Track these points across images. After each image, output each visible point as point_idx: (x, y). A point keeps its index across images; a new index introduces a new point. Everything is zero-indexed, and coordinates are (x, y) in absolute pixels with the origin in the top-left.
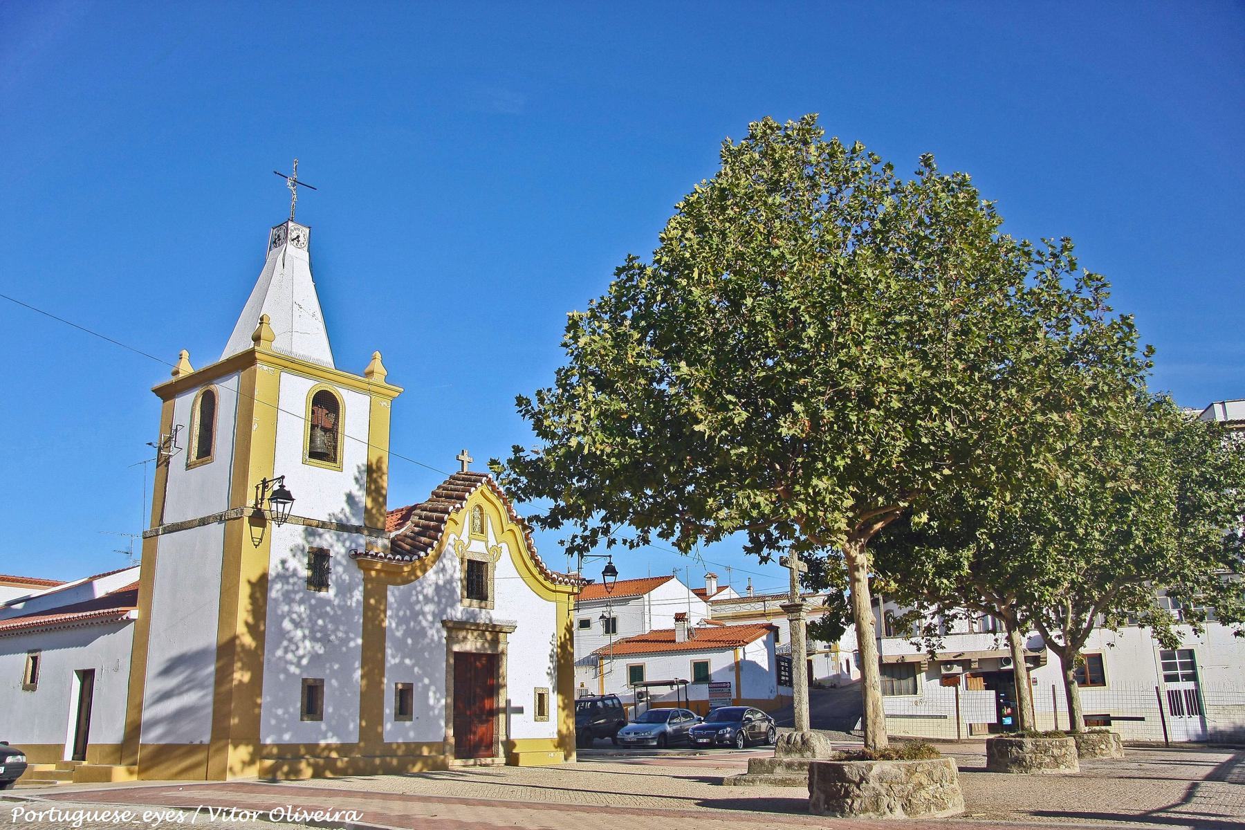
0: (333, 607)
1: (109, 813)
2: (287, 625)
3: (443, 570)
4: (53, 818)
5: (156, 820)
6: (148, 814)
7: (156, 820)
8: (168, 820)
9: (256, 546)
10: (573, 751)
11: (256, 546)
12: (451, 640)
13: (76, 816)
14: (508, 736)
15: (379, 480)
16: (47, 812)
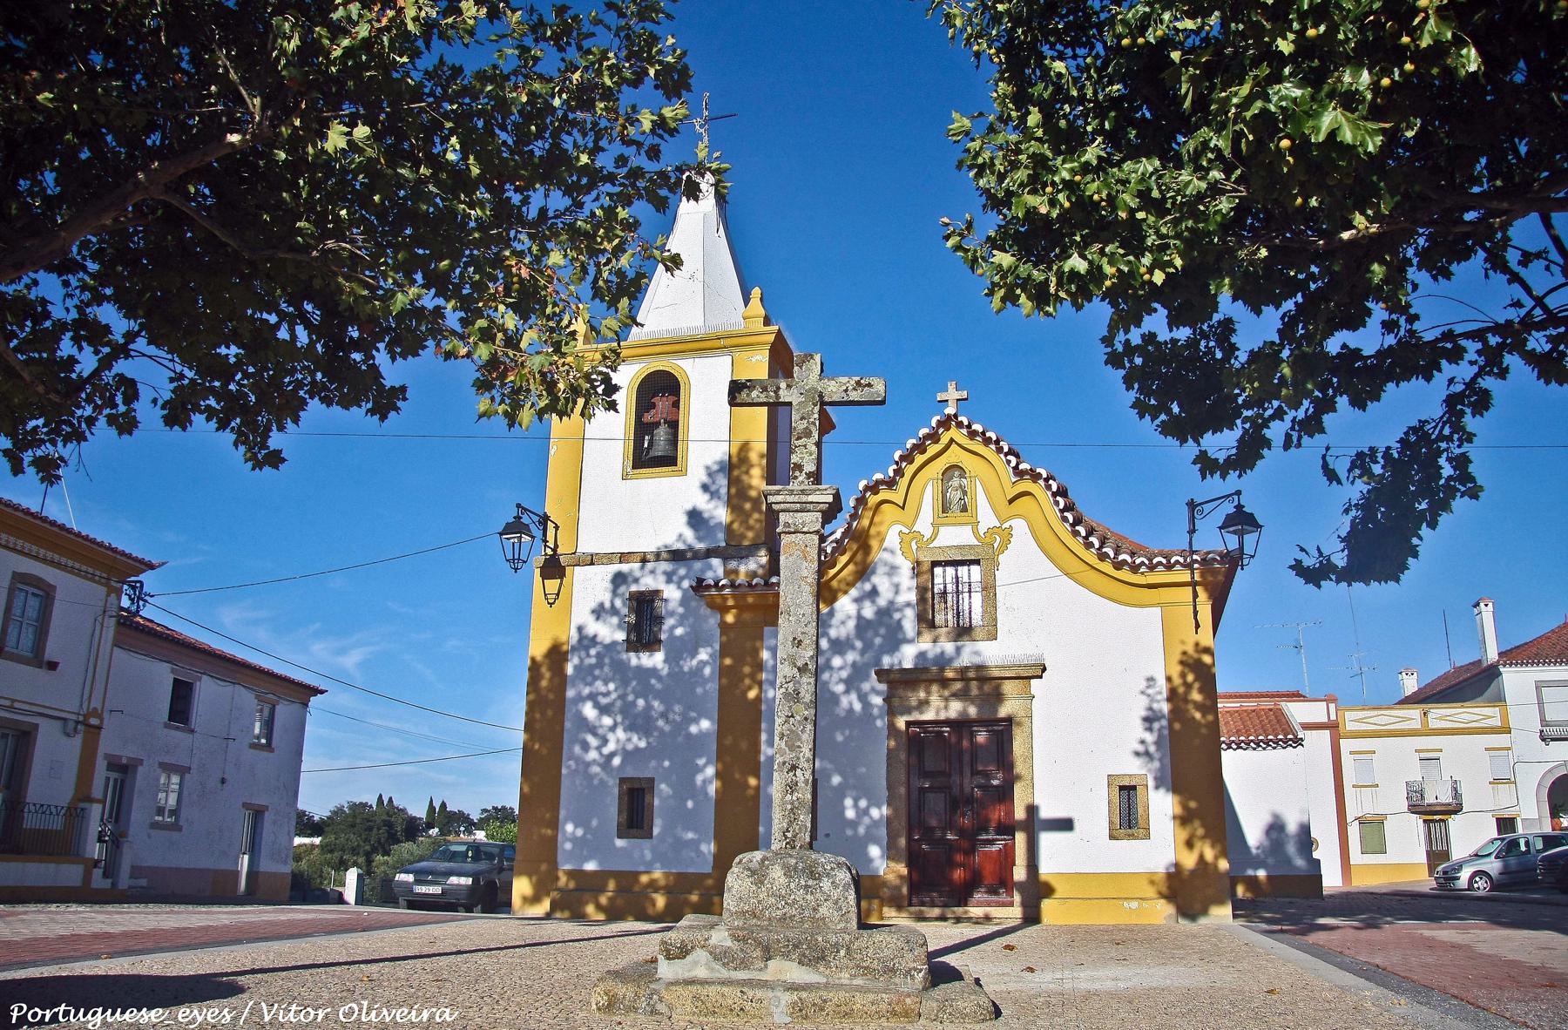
0: (660, 678)
1: (217, 1012)
2: (589, 711)
3: (874, 593)
4: (64, 1018)
5: (194, 1019)
6: (403, 1012)
7: (194, 1019)
8: (399, 1020)
9: (551, 604)
10: (600, 863)
11: (551, 604)
12: (893, 707)
13: (93, 1016)
14: (1032, 866)
15: (745, 478)
16: (56, 1010)
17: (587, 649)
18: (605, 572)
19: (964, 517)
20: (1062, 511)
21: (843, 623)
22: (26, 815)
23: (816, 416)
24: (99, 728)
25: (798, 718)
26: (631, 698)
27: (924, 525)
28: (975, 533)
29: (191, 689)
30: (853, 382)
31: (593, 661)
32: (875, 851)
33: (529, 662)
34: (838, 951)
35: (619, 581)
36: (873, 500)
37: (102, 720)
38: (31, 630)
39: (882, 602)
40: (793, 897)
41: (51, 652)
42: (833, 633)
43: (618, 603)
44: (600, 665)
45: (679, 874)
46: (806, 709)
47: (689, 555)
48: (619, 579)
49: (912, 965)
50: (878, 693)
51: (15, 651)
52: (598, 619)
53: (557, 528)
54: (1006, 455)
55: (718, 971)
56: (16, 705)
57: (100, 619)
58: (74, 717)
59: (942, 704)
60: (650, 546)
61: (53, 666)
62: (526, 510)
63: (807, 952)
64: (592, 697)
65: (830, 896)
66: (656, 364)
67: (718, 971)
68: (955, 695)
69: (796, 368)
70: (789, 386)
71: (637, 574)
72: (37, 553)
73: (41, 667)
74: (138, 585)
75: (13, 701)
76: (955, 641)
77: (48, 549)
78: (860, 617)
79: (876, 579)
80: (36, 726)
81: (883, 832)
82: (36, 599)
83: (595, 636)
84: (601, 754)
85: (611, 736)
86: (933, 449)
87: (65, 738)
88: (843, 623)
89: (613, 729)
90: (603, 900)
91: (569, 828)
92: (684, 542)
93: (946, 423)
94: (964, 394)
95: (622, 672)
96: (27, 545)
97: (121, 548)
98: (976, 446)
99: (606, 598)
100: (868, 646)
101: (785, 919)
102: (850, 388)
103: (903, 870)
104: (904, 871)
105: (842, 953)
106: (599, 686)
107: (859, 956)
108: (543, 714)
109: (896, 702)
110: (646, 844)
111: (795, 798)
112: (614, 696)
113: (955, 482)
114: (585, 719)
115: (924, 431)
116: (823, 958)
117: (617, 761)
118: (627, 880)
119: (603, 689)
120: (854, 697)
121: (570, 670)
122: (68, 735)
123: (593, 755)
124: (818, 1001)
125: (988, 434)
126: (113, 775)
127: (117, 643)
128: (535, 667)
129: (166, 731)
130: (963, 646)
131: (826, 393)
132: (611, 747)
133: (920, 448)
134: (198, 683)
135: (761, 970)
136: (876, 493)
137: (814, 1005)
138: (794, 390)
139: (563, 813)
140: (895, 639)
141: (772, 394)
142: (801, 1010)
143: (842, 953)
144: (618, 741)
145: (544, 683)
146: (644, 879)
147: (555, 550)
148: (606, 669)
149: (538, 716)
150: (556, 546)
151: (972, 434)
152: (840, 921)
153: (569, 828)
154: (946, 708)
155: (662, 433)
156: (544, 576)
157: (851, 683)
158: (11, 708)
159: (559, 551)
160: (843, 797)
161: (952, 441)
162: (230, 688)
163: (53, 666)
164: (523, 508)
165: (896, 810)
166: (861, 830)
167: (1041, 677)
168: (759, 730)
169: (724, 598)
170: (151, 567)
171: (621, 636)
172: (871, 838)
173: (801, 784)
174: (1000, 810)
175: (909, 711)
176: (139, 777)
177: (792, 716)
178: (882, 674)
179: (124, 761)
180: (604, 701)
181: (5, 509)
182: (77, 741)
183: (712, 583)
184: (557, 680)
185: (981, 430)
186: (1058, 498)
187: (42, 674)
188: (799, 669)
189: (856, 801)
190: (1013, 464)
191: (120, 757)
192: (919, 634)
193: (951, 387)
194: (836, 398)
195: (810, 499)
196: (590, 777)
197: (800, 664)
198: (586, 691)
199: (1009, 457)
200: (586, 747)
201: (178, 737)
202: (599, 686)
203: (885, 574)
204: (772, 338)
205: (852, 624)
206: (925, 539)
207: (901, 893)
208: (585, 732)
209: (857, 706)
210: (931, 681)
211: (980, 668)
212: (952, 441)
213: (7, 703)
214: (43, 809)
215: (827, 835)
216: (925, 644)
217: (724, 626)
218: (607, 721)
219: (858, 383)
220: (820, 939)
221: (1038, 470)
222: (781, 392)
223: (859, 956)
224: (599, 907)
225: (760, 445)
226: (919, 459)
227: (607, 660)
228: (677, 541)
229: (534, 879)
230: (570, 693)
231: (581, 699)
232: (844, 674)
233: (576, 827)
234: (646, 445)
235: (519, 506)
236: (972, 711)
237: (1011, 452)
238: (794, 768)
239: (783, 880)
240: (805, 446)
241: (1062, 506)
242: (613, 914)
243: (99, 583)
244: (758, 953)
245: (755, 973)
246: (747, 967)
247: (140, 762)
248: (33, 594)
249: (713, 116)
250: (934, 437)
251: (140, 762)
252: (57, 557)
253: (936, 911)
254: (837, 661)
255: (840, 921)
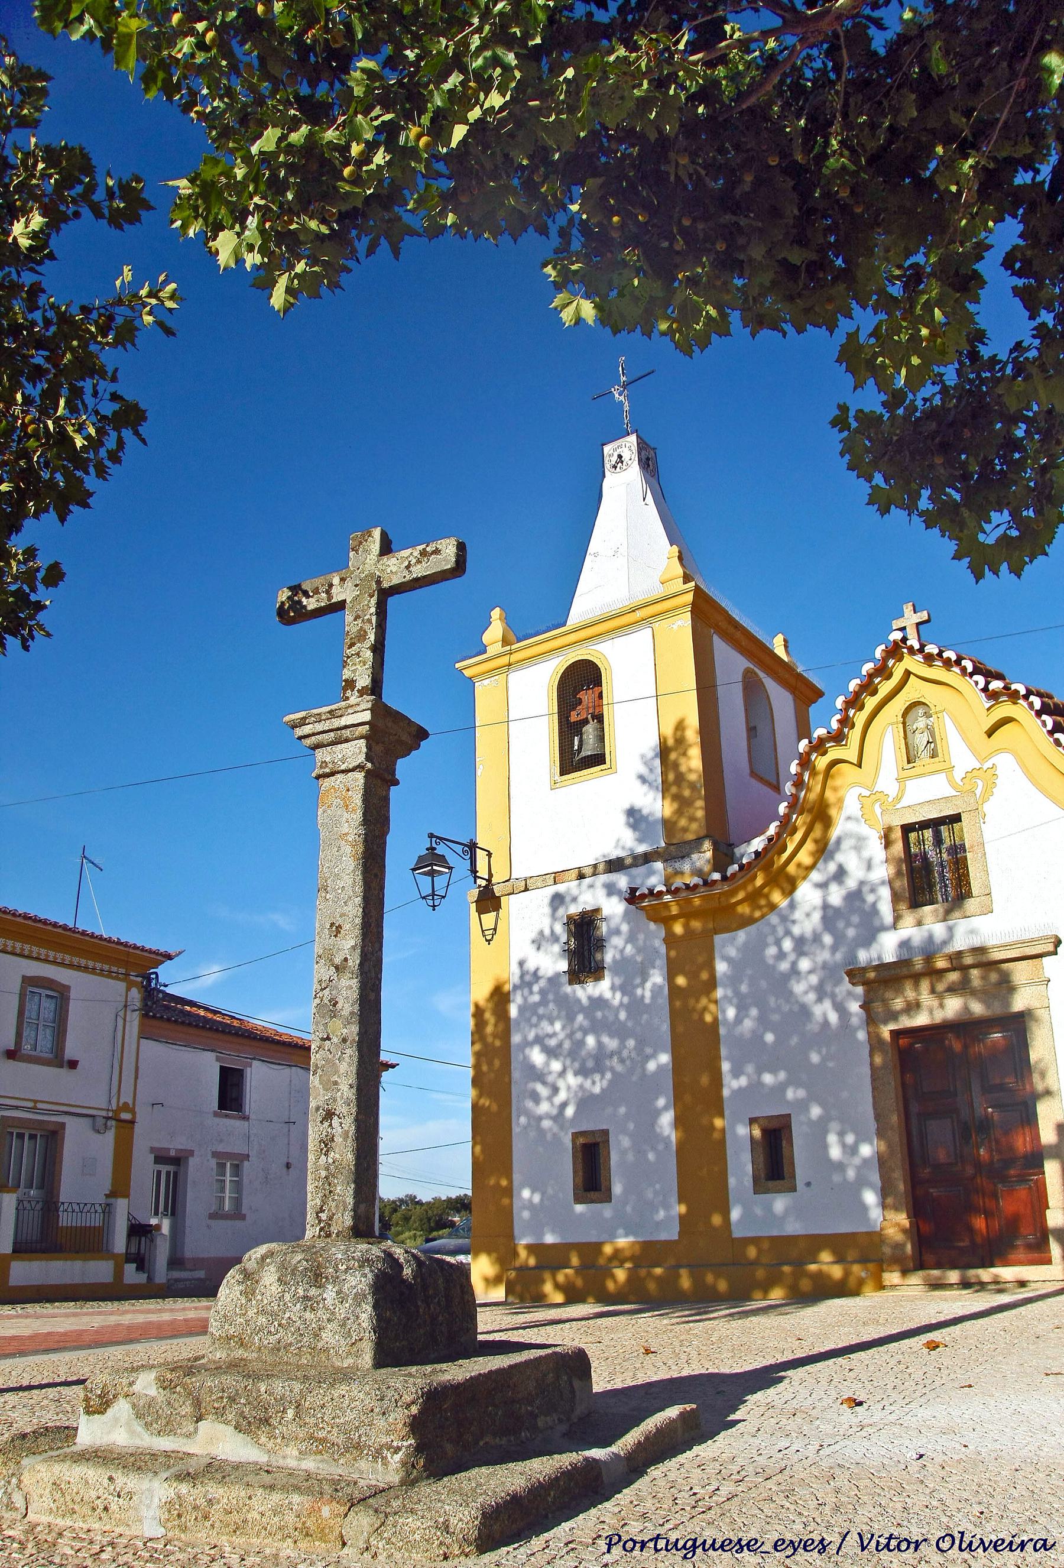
2: (537, 1057)
3: (840, 874)
9: (489, 941)
11: (489, 941)
17: (530, 985)
18: (541, 897)
19: (935, 764)
20: (1051, 733)
21: (808, 915)
22: (60, 1214)
23: (373, 610)
24: (132, 1122)
25: (335, 1040)
26: (579, 1035)
27: (887, 782)
28: (951, 782)
29: (242, 1075)
30: (416, 553)
31: (536, 998)
32: (870, 1197)
33: (472, 1009)
34: (284, 1411)
35: (557, 902)
36: (821, 762)
37: (134, 1113)
38: (48, 1031)
39: (851, 883)
40: (287, 1315)
41: (69, 1053)
42: (796, 930)
43: (559, 928)
44: (544, 1002)
45: (644, 1242)
46: (345, 1027)
47: (628, 861)
48: (558, 900)
49: (385, 1439)
50: (855, 997)
51: (33, 1053)
52: (538, 948)
53: (490, 855)
54: (971, 675)
55: (139, 1436)
56: (39, 1106)
57: (122, 1013)
58: (104, 1113)
59: (935, 1003)
60: (586, 859)
61: (73, 1064)
62: (441, 839)
63: (246, 1410)
64: (539, 1040)
65: (333, 1313)
66: (573, 654)
67: (139, 1436)
68: (952, 990)
69: (352, 554)
70: (343, 580)
71: (575, 892)
72: (63, 959)
73: (61, 1066)
74: (153, 976)
75: (36, 1102)
76: (945, 920)
77: (72, 955)
78: (826, 906)
79: (840, 857)
80: (63, 1125)
81: (875, 1178)
82: (49, 1000)
83: (537, 970)
84: (552, 1104)
85: (561, 1084)
86: (885, 688)
87: (98, 1135)
88: (808, 915)
89: (562, 1074)
90: (561, 1278)
91: (526, 1193)
92: (623, 848)
93: (895, 651)
94: (924, 616)
95: (569, 1008)
96: (35, 949)
97: (131, 942)
98: (937, 672)
99: (545, 924)
100: (839, 939)
101: (278, 1350)
102: (414, 561)
103: (902, 1219)
104: (906, 1223)
105: (290, 1413)
106: (546, 1028)
107: (312, 1421)
108: (490, 1064)
109: (878, 1007)
110: (607, 1211)
111: (330, 1161)
112: (561, 1036)
113: (921, 723)
114: (532, 1067)
115: (868, 667)
116: (266, 1421)
117: (570, 1111)
118: (590, 1251)
119: (549, 1029)
120: (827, 1005)
121: (513, 1011)
122: (99, 1132)
123: (544, 1107)
124: (201, 1502)
125: (945, 655)
126: (164, 1169)
127: (144, 1035)
128: (478, 1013)
129: (217, 1120)
130: (955, 924)
131: (384, 577)
132: (562, 1096)
133: (868, 687)
134: (249, 1069)
135: (189, 1436)
136: (824, 753)
137: (196, 1508)
138: (349, 584)
139: (517, 1177)
140: (870, 931)
141: (324, 595)
142: (179, 1516)
143: (290, 1413)
144: (569, 1088)
145: (489, 1029)
146: (608, 1249)
147: (489, 881)
148: (551, 1006)
149: (485, 1068)
150: (491, 875)
151: (929, 659)
152: (349, 1353)
153: (526, 1193)
154: (942, 1006)
155: (590, 730)
156: (481, 911)
157: (821, 993)
158: (34, 1109)
159: (494, 881)
160: (825, 1132)
161: (908, 674)
162: (287, 1071)
163: (73, 1064)
164: (437, 837)
165: (890, 1146)
166: (851, 1174)
167: (1055, 953)
168: (718, 1058)
169: (666, 905)
170: (169, 957)
171: (563, 966)
172: (861, 1182)
173: (338, 1139)
174: (1024, 1134)
175: (894, 1016)
176: (191, 1169)
177: (328, 1038)
178: (855, 974)
179: (172, 1153)
180: (553, 1042)
181: (4, 916)
182: (110, 1136)
183: (646, 892)
184: (501, 1027)
185: (936, 651)
186: (1044, 717)
187: (64, 1072)
188: (337, 968)
189: (841, 1134)
190: (982, 685)
191: (169, 1149)
192: (897, 918)
193: (908, 609)
194: (396, 580)
195: (343, 721)
196: (542, 1132)
197: (338, 960)
198: (531, 1036)
199: (976, 677)
200: (536, 1098)
201: (231, 1124)
202: (546, 1028)
203: (851, 848)
204: (689, 597)
205: (817, 916)
206: (890, 799)
207: (904, 1253)
208: (534, 1081)
209: (833, 1017)
210: (916, 978)
211: (980, 950)
212: (908, 674)
213: (30, 1104)
214: (83, 1207)
215: (808, 1184)
216: (909, 930)
217: (670, 940)
218: (556, 1066)
219: (423, 553)
220: (263, 1389)
221: (1014, 687)
222: (334, 591)
223: (312, 1421)
224: (557, 1286)
225: (693, 721)
226: (871, 703)
227: (551, 997)
228: (616, 847)
229: (494, 1255)
230: (516, 1039)
231: (527, 1044)
232: (814, 979)
233: (533, 1192)
234: (576, 747)
235: (431, 836)
236: (977, 1008)
237: (977, 671)
238: (329, 1115)
239: (275, 1289)
240: (358, 654)
241: (1050, 726)
242: (573, 1296)
243: (117, 978)
244: (187, 1409)
245: (183, 1440)
246: (172, 1432)
247: (191, 1153)
248: (47, 996)
249: (631, 380)
250: (883, 671)
251: (191, 1153)
252: (76, 960)
253: (954, 1276)
254: (804, 964)
255: (349, 1353)
